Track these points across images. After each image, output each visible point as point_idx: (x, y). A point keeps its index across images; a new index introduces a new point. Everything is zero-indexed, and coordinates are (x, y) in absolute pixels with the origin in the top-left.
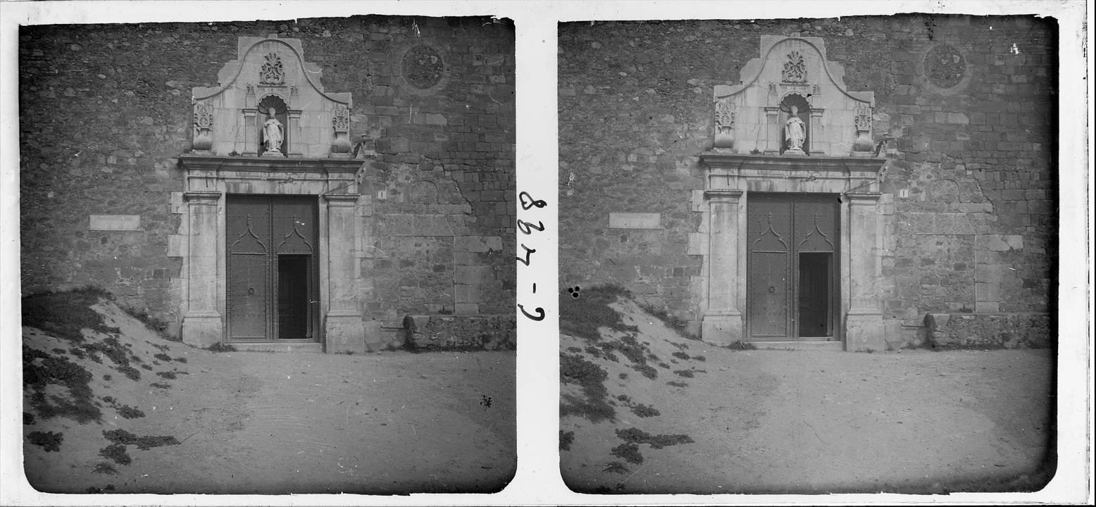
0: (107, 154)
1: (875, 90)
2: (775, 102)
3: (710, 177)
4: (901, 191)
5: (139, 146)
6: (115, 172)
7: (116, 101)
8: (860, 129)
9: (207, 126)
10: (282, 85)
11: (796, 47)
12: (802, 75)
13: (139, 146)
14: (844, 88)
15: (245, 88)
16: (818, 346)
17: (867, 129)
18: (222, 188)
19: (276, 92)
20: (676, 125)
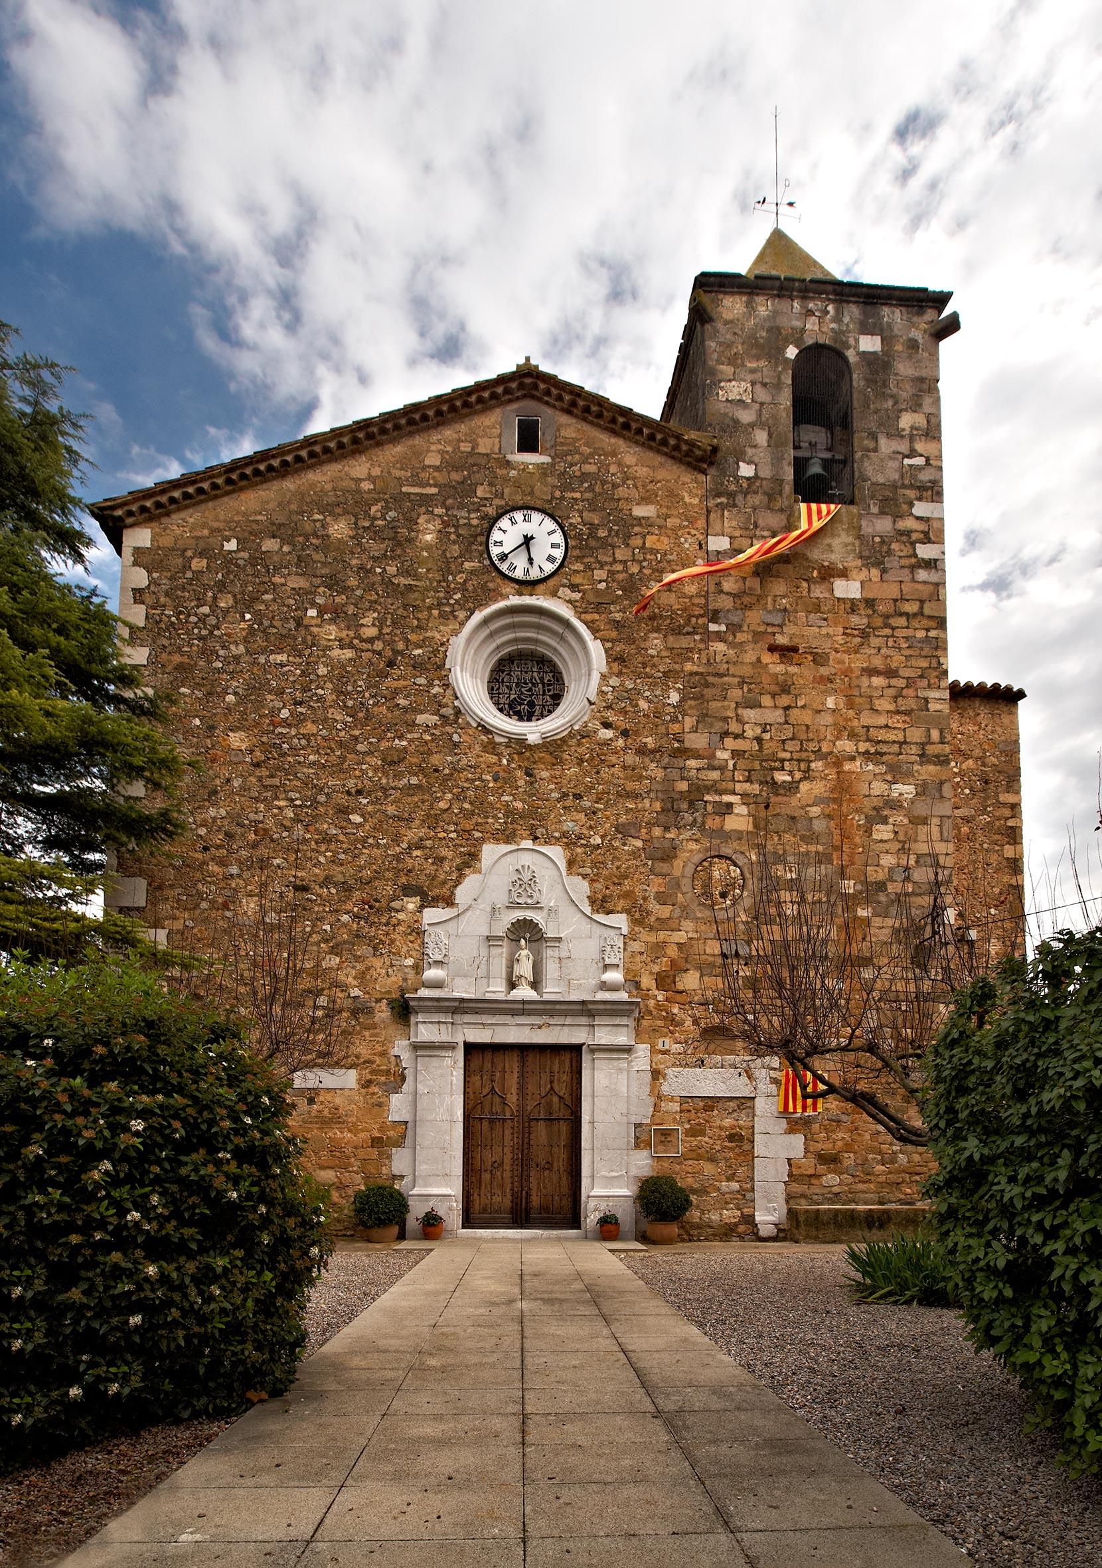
0: (318, 993)
1: (628, 912)
2: (501, 929)
3: (417, 1023)
4: (660, 1041)
5: (355, 983)
6: (327, 1016)
7: (328, 927)
8: (607, 961)
9: (439, 958)
10: (536, 907)
11: (526, 859)
12: (534, 894)
13: (355, 983)
14: (587, 910)
15: (489, 909)
16: (559, 1239)
17: (615, 961)
18: (460, 1039)
19: (529, 914)
20: (374, 959)
